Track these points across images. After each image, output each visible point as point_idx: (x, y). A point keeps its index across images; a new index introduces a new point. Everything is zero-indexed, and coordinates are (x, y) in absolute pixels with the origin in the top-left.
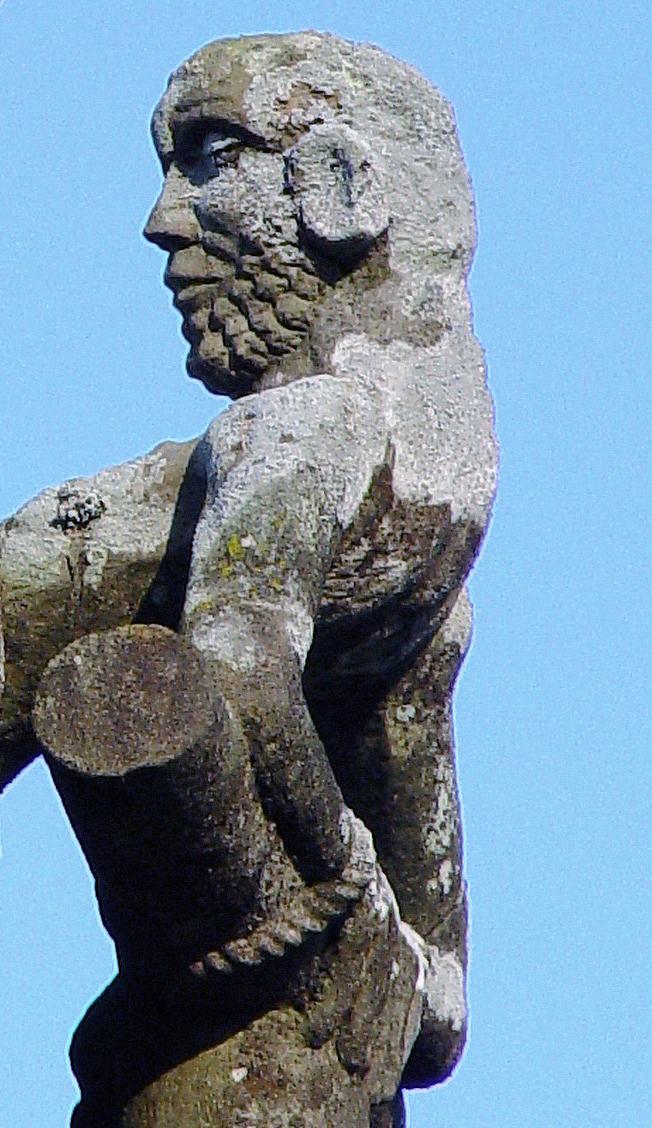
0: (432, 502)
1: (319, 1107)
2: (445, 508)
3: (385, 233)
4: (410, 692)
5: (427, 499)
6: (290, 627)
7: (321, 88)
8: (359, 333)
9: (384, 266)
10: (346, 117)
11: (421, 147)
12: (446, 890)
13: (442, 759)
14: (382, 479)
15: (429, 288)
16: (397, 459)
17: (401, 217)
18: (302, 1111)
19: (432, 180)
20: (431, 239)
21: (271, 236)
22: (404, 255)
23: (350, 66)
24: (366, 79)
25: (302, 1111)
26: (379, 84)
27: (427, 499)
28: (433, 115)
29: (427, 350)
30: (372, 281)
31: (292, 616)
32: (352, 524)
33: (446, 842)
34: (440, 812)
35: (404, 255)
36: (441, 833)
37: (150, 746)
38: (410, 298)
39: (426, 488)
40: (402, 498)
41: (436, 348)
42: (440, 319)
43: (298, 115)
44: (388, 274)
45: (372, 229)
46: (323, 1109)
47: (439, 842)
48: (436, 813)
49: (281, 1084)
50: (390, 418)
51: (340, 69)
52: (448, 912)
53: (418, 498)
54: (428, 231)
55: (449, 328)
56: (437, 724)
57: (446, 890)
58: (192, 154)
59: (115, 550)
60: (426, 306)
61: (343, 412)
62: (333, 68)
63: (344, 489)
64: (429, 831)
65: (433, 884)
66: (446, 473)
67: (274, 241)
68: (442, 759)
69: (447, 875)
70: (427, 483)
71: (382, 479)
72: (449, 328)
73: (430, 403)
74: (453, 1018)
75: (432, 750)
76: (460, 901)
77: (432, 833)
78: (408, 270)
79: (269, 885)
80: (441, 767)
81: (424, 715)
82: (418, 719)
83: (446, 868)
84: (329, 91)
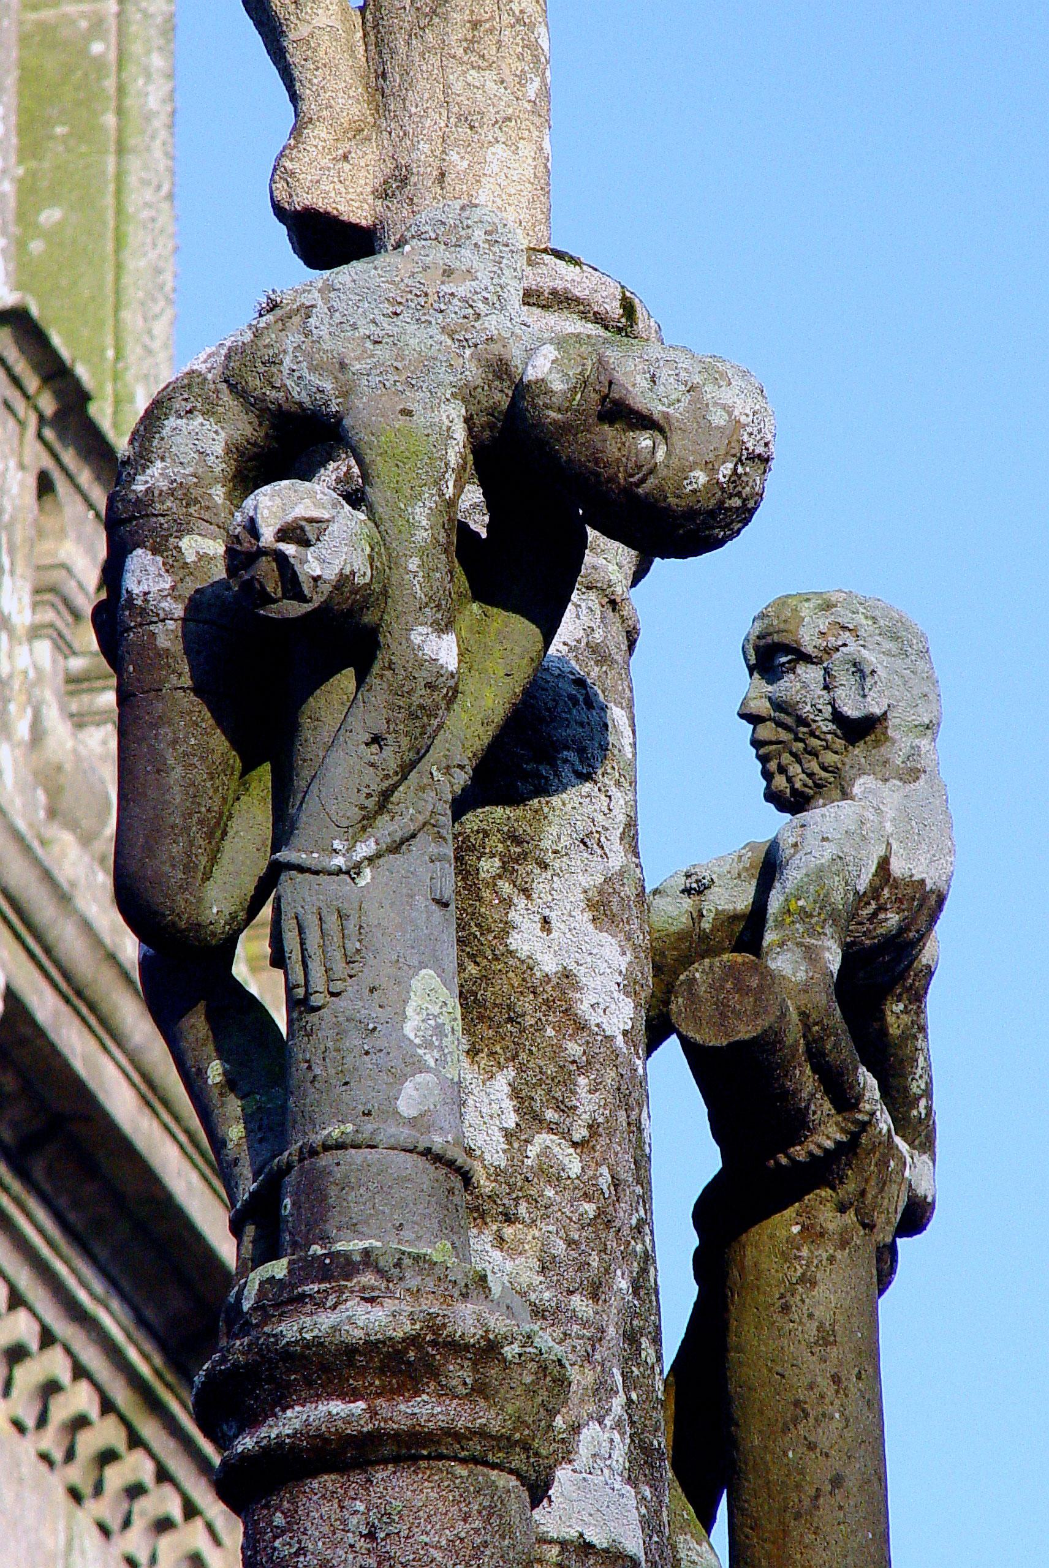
3: (885, 713)
5: (911, 876)
9: (885, 733)
10: (862, 642)
11: (908, 661)
12: (923, 1116)
14: (884, 864)
15: (912, 748)
19: (914, 681)
26: (882, 622)
27: (911, 876)
28: (915, 641)
30: (877, 743)
33: (923, 1086)
35: (897, 727)
37: (742, 1028)
43: (832, 642)
44: (887, 738)
45: (877, 711)
47: (918, 1087)
49: (822, 1235)
50: (889, 827)
55: (925, 772)
57: (923, 1116)
59: (720, 908)
62: (854, 613)
65: (915, 1112)
67: (817, 718)
71: (884, 864)
79: (815, 1113)
82: (906, 1011)
83: (923, 1103)
84: (851, 626)
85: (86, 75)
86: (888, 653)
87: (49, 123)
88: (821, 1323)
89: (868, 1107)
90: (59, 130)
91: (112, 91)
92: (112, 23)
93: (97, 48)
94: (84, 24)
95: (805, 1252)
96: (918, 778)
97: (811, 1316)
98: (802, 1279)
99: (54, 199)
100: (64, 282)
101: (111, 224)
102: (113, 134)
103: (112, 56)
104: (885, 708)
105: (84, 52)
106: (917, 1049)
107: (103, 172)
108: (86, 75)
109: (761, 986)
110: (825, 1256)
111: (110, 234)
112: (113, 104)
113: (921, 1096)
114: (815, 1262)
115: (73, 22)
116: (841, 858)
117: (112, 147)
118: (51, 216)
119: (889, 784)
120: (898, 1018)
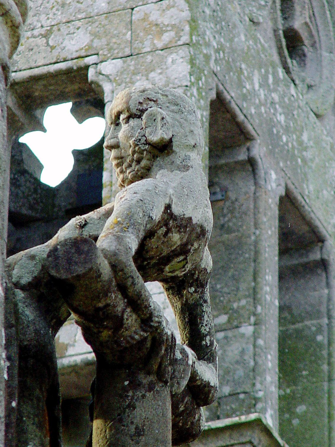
0: (186, 216)
1: (151, 392)
2: (190, 218)
3: (171, 139)
4: (193, 282)
5: (184, 215)
6: (128, 239)
7: (152, 99)
8: (165, 169)
9: (172, 149)
10: (160, 106)
11: (183, 115)
12: (208, 345)
13: (205, 305)
14: (168, 207)
15: (185, 155)
16: (173, 202)
17: (176, 134)
18: (145, 393)
19: (186, 124)
20: (186, 141)
21: (138, 142)
22: (178, 146)
23: (161, 92)
24: (167, 96)
25: (145, 393)
26: (170, 97)
27: (184, 215)
28: (187, 106)
29: (185, 173)
30: (168, 154)
31: (129, 237)
32: (159, 221)
33: (208, 330)
34: (205, 321)
35: (178, 146)
36: (206, 327)
37: (79, 269)
38: (180, 158)
39: (183, 212)
40: (176, 214)
41: (187, 172)
42: (189, 165)
43: (145, 106)
44: (173, 152)
45: (167, 137)
46: (152, 392)
47: (205, 330)
48: (204, 321)
49: (139, 385)
50: (171, 191)
51: (158, 93)
52: (209, 352)
53: (181, 215)
54: (185, 139)
55: (192, 167)
56: (202, 293)
57: (208, 345)
58: (118, 122)
59: (91, 234)
60: (185, 161)
61: (155, 187)
62: (156, 93)
63: (153, 208)
64: (202, 326)
65: (204, 343)
66: (190, 208)
67: (139, 143)
68: (205, 305)
69: (208, 340)
70: (184, 210)
71: (168, 207)
72: (192, 167)
73: (184, 187)
74: (210, 381)
75: (201, 302)
76: (214, 348)
77: (203, 327)
78: (179, 150)
79: (127, 319)
80: (205, 307)
81: (197, 291)
82: (195, 292)
83: (208, 338)
84: (155, 99)
85: (315, 350)
86: (173, 111)
87: (300, 370)
88: (137, 425)
89: (157, 319)
90: (305, 373)
91: (326, 356)
92: (325, 328)
93: (319, 338)
94: (314, 329)
95: (130, 394)
96: (188, 170)
97: (132, 423)
98: (129, 406)
99: (302, 401)
100: (307, 436)
101: (327, 411)
102: (327, 373)
103: (326, 342)
104: (171, 136)
105: (314, 340)
106: (203, 311)
107: (323, 390)
108: (315, 350)
109: (89, 250)
110: (140, 394)
111: (326, 415)
112: (326, 361)
113: (207, 335)
114: (136, 398)
115: (310, 328)
116: (141, 200)
117: (326, 379)
118: (301, 409)
119: (174, 173)
120: (192, 295)
